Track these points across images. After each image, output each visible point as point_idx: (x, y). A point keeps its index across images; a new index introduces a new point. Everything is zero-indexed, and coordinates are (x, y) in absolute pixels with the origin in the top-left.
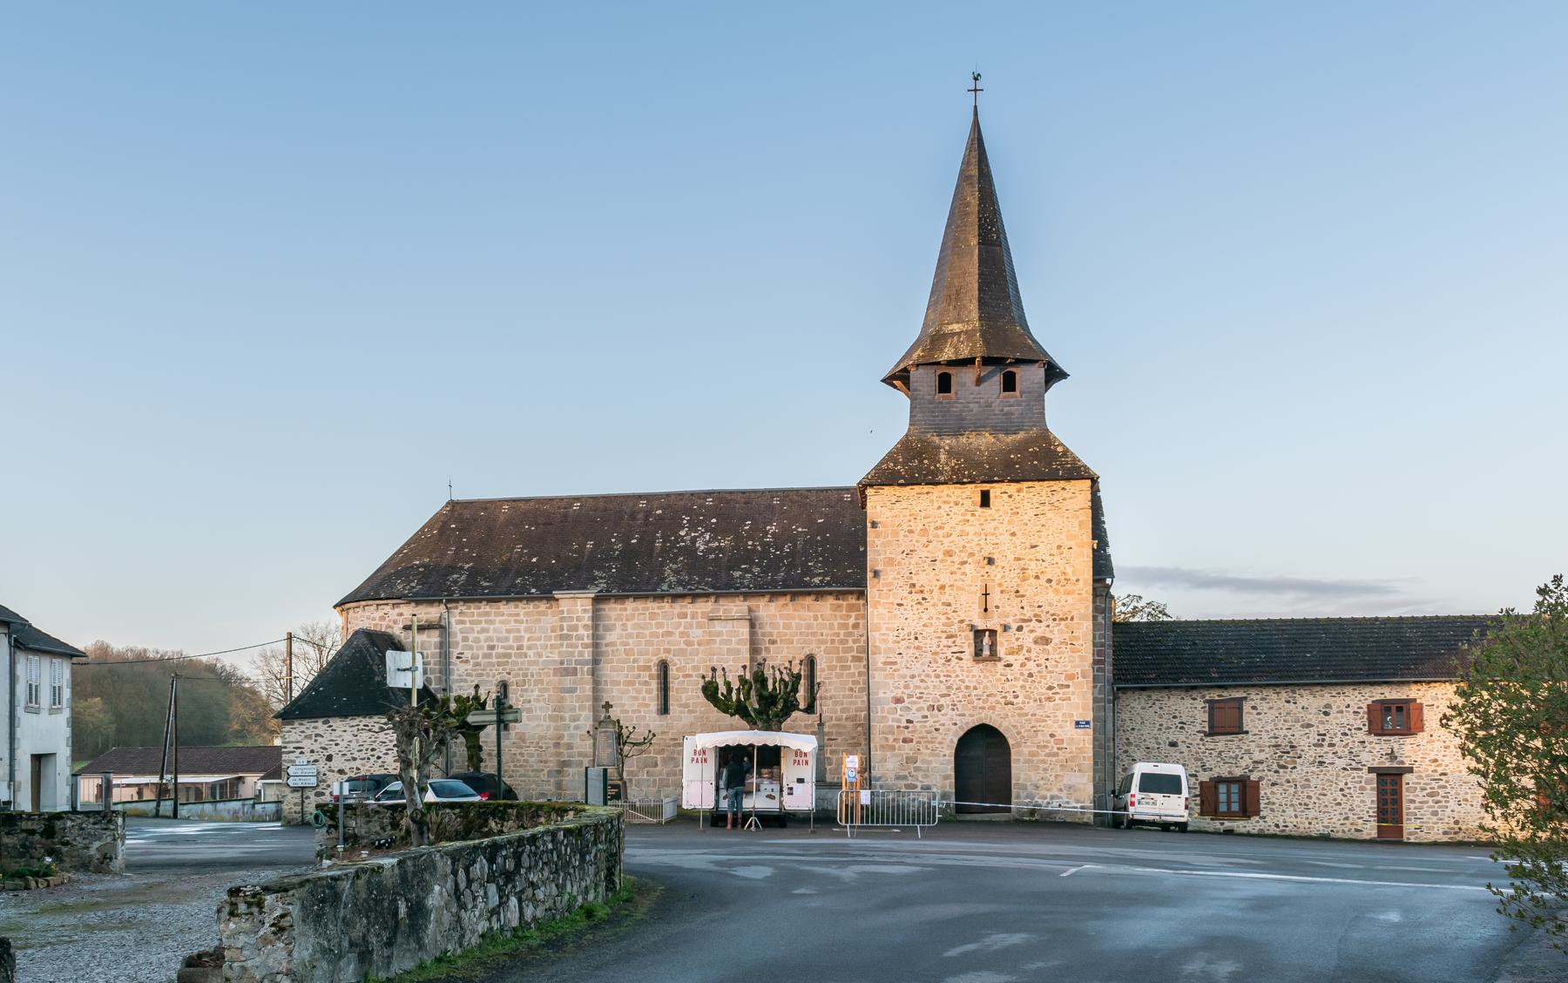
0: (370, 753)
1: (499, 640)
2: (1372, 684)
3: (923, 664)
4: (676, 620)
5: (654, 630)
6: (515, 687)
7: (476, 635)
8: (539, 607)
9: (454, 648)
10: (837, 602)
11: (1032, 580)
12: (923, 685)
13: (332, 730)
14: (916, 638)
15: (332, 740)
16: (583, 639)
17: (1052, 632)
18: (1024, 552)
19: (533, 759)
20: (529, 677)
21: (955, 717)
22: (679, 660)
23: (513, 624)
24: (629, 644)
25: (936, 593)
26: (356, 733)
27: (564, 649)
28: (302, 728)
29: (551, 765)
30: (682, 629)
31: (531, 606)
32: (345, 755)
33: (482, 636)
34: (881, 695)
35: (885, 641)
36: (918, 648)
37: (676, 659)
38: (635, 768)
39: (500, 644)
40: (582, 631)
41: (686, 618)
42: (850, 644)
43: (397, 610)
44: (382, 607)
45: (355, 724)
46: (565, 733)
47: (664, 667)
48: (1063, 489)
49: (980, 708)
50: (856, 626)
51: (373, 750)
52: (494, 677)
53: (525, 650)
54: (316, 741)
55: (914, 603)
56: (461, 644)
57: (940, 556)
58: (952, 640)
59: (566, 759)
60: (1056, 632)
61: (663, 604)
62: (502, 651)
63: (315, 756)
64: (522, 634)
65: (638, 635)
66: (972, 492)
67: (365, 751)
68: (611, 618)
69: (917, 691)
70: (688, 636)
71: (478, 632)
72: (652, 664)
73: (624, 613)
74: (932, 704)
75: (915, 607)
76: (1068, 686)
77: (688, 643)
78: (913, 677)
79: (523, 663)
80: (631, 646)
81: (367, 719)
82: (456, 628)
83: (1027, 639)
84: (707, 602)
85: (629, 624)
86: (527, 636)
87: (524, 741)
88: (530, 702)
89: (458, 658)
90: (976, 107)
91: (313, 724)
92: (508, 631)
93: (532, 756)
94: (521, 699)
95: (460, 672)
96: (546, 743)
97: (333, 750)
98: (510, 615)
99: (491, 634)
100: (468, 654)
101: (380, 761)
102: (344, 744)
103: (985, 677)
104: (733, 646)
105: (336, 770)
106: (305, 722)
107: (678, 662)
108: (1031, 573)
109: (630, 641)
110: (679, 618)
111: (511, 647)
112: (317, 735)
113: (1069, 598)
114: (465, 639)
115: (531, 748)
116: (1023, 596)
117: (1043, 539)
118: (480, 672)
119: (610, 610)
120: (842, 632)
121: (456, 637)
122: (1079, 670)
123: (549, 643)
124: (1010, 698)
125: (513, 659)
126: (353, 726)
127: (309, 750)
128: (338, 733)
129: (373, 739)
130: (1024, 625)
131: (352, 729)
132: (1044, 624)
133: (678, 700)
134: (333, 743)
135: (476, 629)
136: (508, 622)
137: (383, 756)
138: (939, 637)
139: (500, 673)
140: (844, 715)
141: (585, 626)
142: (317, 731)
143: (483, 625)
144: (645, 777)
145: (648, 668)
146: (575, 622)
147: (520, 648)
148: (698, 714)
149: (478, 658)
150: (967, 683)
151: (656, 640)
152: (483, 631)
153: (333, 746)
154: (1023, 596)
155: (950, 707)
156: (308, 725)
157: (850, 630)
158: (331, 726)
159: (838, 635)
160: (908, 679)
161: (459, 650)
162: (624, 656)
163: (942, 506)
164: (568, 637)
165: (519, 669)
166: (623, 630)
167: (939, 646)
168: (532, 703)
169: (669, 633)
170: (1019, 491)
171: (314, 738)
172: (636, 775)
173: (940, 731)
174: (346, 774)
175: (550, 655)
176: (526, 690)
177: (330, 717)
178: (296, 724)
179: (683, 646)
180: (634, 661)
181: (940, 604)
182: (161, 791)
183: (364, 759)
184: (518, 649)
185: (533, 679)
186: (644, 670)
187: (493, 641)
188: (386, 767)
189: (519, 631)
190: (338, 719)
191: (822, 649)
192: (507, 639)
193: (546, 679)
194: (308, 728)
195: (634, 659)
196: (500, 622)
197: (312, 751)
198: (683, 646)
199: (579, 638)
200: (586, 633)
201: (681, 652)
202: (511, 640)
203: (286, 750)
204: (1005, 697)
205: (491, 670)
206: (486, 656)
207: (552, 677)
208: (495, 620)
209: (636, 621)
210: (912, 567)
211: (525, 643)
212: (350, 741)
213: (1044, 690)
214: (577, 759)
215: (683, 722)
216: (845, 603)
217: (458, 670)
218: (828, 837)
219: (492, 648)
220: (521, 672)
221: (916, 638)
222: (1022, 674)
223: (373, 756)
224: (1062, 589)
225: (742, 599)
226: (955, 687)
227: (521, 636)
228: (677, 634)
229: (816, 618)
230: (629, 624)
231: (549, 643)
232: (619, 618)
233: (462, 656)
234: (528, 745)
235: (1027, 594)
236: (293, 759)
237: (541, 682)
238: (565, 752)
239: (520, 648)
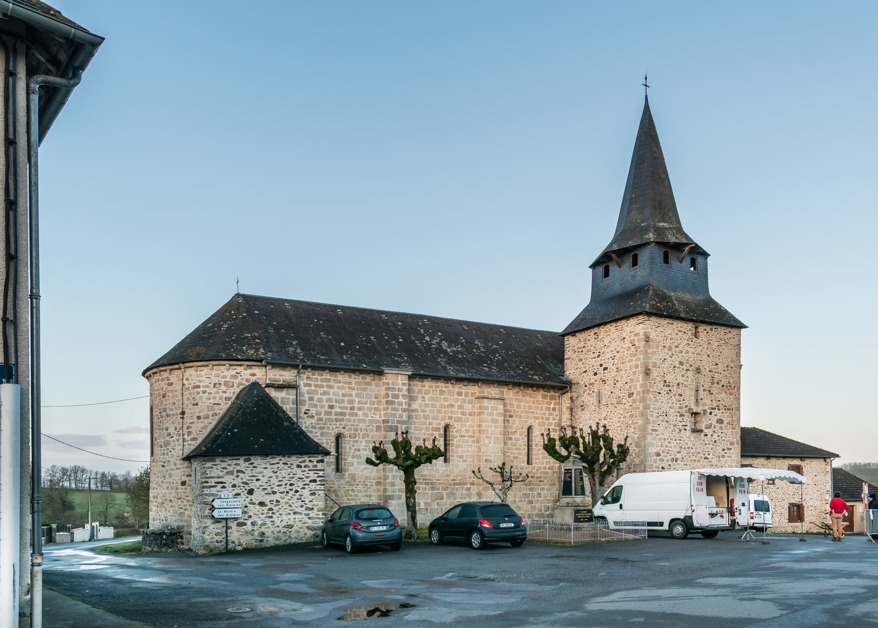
0: (289, 487)
1: (337, 401)
2: (784, 458)
3: (669, 432)
4: (456, 396)
5: (442, 402)
6: (348, 439)
7: (319, 396)
8: (366, 379)
9: (302, 405)
10: (545, 393)
11: (716, 385)
12: (669, 445)
13: (254, 467)
14: (666, 415)
15: (254, 476)
16: (402, 406)
17: (724, 416)
18: (713, 367)
19: (361, 494)
20: (359, 432)
21: (683, 466)
22: (458, 425)
23: (347, 390)
24: (426, 412)
25: (675, 387)
26: (276, 470)
27: (389, 411)
28: (224, 465)
29: (374, 498)
30: (459, 403)
31: (360, 378)
32: (266, 489)
33: (324, 398)
34: (650, 451)
35: (652, 416)
36: (667, 422)
37: (455, 424)
38: (429, 501)
39: (338, 405)
40: (401, 399)
41: (462, 395)
42: (551, 421)
43: (250, 371)
44: (234, 367)
45: (275, 462)
46: (390, 474)
47: (447, 428)
48: (730, 332)
50: (554, 409)
51: (291, 485)
52: (333, 430)
53: (356, 411)
54: (238, 476)
55: (665, 393)
56: (308, 402)
57: (677, 365)
58: (682, 418)
59: (390, 494)
60: (725, 417)
61: (448, 385)
62: (339, 410)
63: (237, 491)
64: (354, 398)
65: (432, 406)
66: (690, 326)
67: (284, 486)
68: (414, 391)
69: (667, 449)
70: (463, 408)
71: (321, 394)
72: (441, 427)
73: (423, 389)
75: (666, 395)
76: (731, 449)
77: (463, 414)
78: (665, 440)
79: (354, 421)
80: (428, 413)
81: (286, 458)
82: (304, 389)
83: (714, 420)
84: (474, 386)
85: (427, 397)
86: (357, 400)
87: (354, 480)
88: (359, 450)
89: (305, 413)
90: (646, 96)
91: (235, 462)
92: (344, 395)
93: (361, 491)
94: (353, 448)
95: (307, 425)
96: (370, 482)
97: (254, 485)
98: (345, 383)
99: (331, 396)
100: (313, 411)
101: (298, 494)
102: (266, 479)
103: (696, 442)
104: (495, 417)
105: (257, 502)
106: (227, 459)
107: (457, 426)
108: (715, 380)
109: (427, 409)
110: (458, 395)
111: (346, 408)
112: (238, 471)
113: (731, 397)
114: (311, 399)
115: (360, 486)
116: (712, 394)
117: (721, 361)
118: (322, 425)
119: (414, 385)
120: (547, 412)
121: (304, 397)
122: (735, 440)
123: (373, 407)
124: (707, 455)
125: (347, 417)
126: (273, 464)
127: (231, 485)
128: (258, 470)
129: (292, 476)
130: (713, 411)
131: (273, 466)
132: (721, 411)
133: (456, 453)
134: (254, 479)
135: (319, 392)
136: (344, 388)
137: (300, 490)
138: (676, 416)
139: (337, 427)
140: (548, 466)
141: (404, 396)
142: (238, 468)
143: (325, 389)
144: (436, 507)
145: (438, 429)
146: (397, 392)
147: (352, 409)
148: (468, 463)
149: (321, 415)
150: (689, 445)
151: (443, 410)
152: (325, 393)
153: (255, 481)
154: (712, 394)
156: (230, 462)
157: (551, 412)
158: (253, 463)
159: (545, 414)
160: (663, 441)
161: (306, 407)
162: (423, 420)
163: (679, 333)
164: (392, 403)
165: (352, 425)
166: (423, 401)
167: (676, 421)
168: (361, 451)
169: (452, 406)
170: (711, 330)
171: (235, 474)
172: (430, 506)
174: (266, 505)
175: (373, 416)
176: (357, 442)
177: (251, 455)
178: (218, 461)
179: (460, 415)
180: (430, 424)
181: (677, 395)
182: (552, 516)
183: (284, 492)
184: (351, 410)
185: (361, 433)
186: (436, 431)
187: (332, 402)
188: (303, 500)
189: (351, 395)
190: (259, 458)
191: (537, 423)
192: (343, 401)
193: (371, 434)
194: (230, 465)
195: (429, 423)
196: (338, 388)
197: (234, 486)
198: (460, 415)
199: (400, 404)
200: (404, 401)
201: (458, 420)
202: (346, 403)
203: (208, 485)
204: (704, 454)
205: (331, 425)
206: (327, 413)
207: (375, 433)
208: (334, 386)
209: (431, 395)
210: (665, 370)
211: (356, 405)
212: (271, 477)
213: (721, 451)
214: (397, 494)
215: (459, 468)
216: (549, 394)
217: (305, 423)
218: (55, 546)
219: (332, 407)
220: (353, 427)
221: (666, 415)
222: (712, 441)
223: (291, 490)
224: (728, 391)
225: (496, 385)
226: (683, 447)
227: (353, 400)
228: (456, 406)
229: (534, 402)
230: (427, 397)
231: (373, 407)
232: (420, 392)
233: (308, 412)
234: (357, 483)
235: (714, 392)
236: (215, 492)
237: (368, 435)
238: (390, 488)
239: (352, 409)
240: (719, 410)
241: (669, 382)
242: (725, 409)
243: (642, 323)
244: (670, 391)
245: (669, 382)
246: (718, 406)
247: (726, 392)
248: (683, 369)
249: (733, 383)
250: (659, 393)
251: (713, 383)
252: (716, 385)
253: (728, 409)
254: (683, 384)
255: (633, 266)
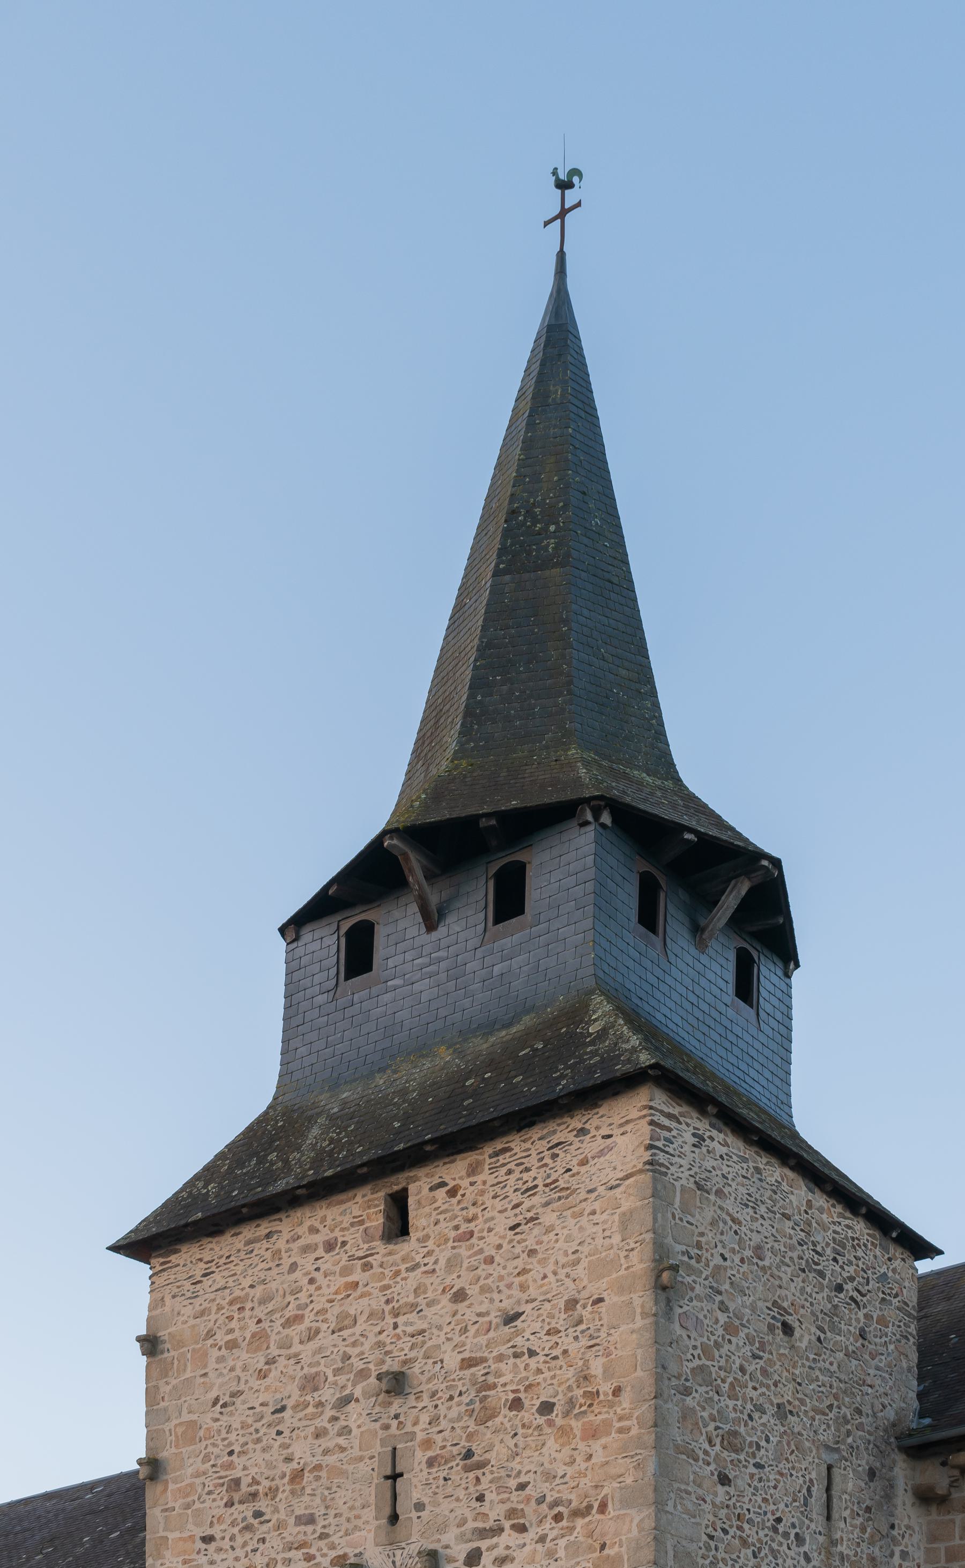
11: (505, 1417)
55: (236, 1530)
90: (561, 256)
132: (532, 1534)
240: (522, 1529)
241: (255, 1482)
242: (558, 1518)
243: (745, 1081)
244: (258, 1514)
245: (255, 1482)
246: (511, 1514)
247: (564, 1433)
248: (320, 1404)
249: (608, 1372)
250: (208, 1539)
251: (486, 1416)
252: (505, 1417)
253: (576, 1513)
254: (318, 1467)
255: (497, 921)
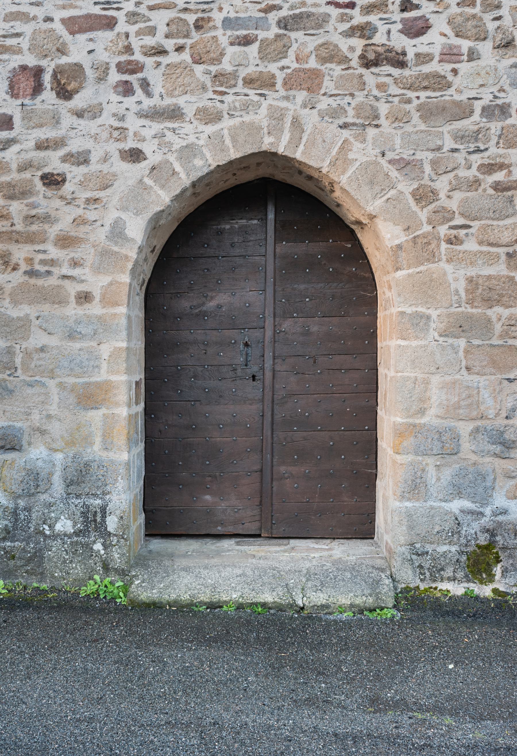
49: (249, 82)
74: (31, 61)
155: (115, 76)
173: (68, 188)
